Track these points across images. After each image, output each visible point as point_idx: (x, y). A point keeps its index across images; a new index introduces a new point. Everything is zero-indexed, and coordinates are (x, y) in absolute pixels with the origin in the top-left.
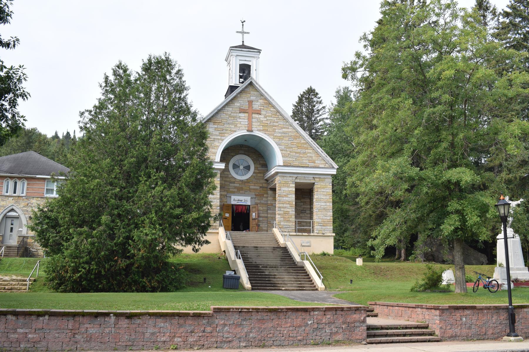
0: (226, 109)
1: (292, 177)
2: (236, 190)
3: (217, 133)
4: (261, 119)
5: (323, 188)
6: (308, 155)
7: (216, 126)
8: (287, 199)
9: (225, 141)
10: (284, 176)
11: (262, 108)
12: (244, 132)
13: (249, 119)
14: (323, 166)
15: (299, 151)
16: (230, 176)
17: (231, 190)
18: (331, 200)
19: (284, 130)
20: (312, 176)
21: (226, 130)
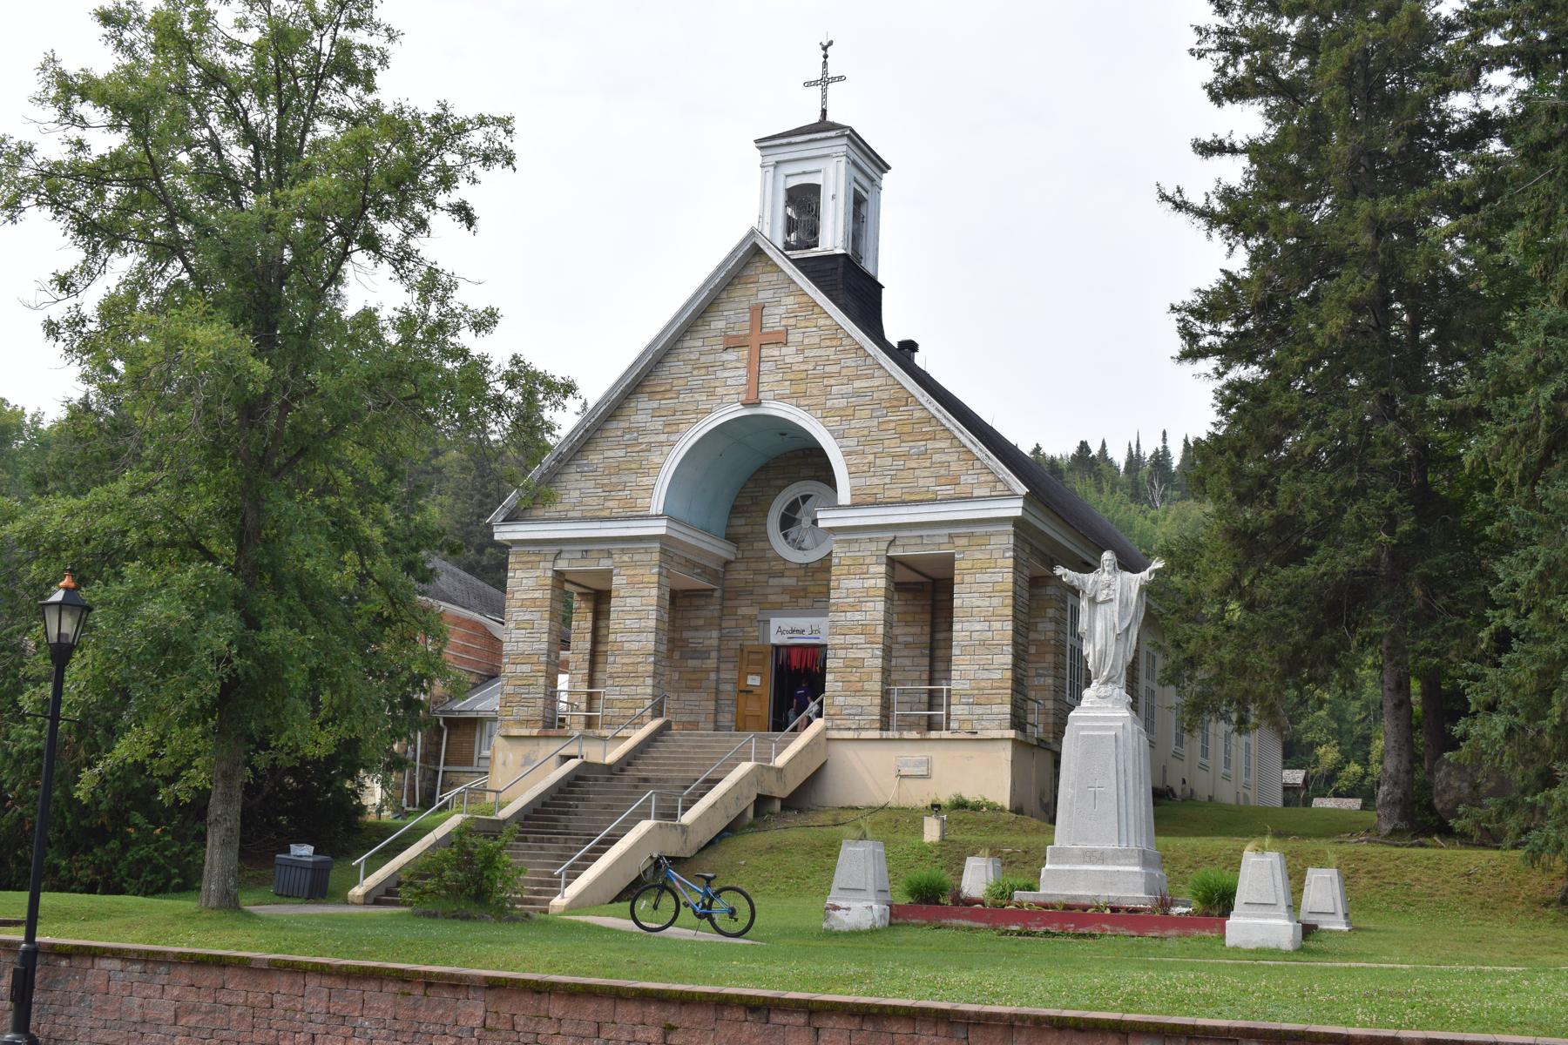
0: (686, 344)
1: (877, 540)
2: (787, 598)
3: (659, 425)
4: (788, 360)
5: (983, 570)
6: (936, 458)
7: (655, 404)
8: (857, 616)
9: (679, 446)
10: (849, 541)
11: (792, 322)
12: (740, 412)
13: (749, 366)
14: (985, 492)
15: (905, 448)
16: (769, 554)
17: (772, 598)
18: (1009, 611)
19: (857, 384)
20: (947, 531)
21: (684, 412)
